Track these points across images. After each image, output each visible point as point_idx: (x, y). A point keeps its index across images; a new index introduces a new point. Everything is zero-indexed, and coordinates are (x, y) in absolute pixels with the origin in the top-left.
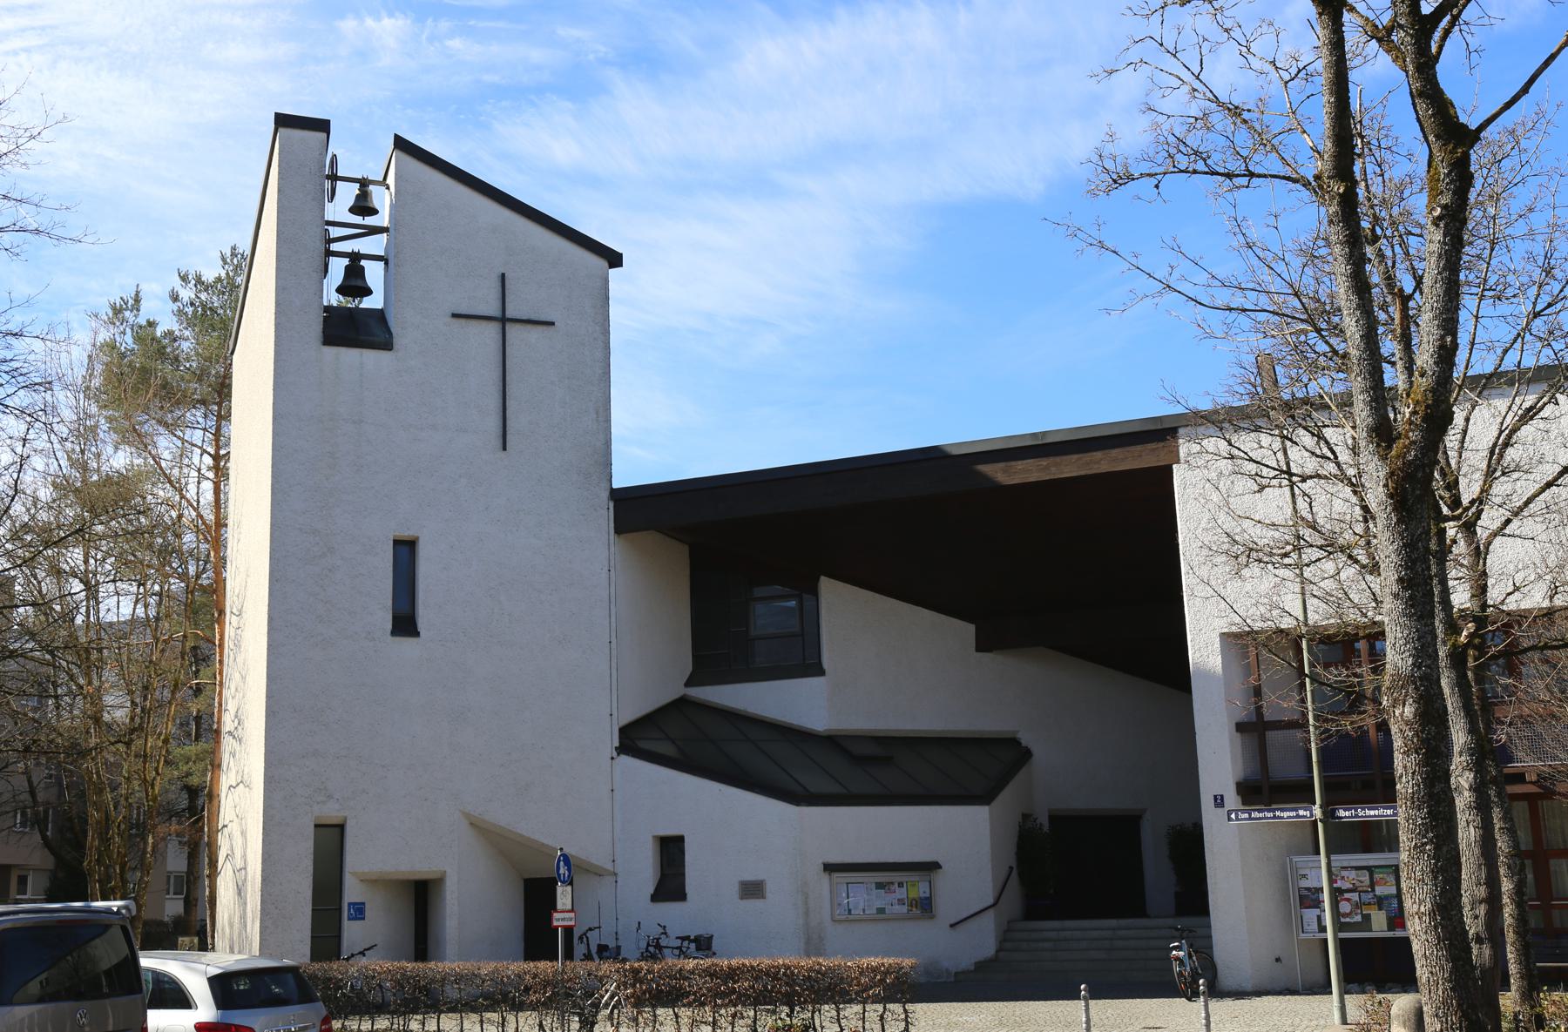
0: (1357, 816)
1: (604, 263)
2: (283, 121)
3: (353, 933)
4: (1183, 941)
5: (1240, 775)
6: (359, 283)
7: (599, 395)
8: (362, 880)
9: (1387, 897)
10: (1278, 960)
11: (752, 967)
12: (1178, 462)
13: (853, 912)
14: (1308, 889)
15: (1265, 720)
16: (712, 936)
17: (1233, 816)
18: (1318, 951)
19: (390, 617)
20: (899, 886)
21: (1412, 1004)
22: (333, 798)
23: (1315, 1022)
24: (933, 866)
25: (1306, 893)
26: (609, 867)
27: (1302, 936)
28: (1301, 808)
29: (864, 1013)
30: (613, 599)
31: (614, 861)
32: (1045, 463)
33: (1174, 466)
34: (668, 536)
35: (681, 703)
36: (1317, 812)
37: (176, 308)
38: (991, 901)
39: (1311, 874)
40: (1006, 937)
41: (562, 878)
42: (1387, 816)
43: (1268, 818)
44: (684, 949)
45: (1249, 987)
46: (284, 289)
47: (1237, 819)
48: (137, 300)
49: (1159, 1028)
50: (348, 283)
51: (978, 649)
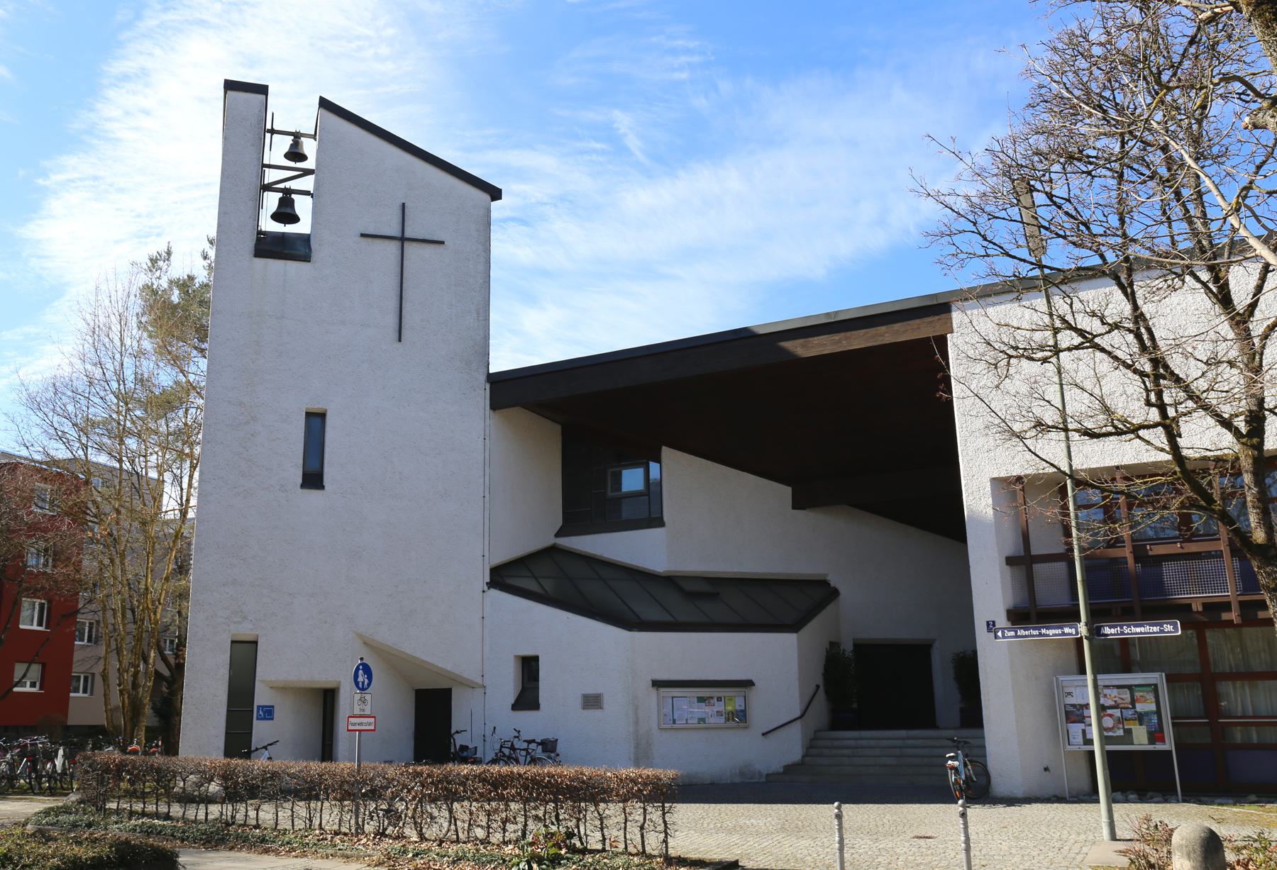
0: (1162, 631)
1: (487, 197)
2: (230, 86)
3: (261, 731)
4: (959, 752)
5: (1010, 603)
6: (289, 211)
7: (480, 299)
8: (271, 687)
9: (1147, 714)
10: (1046, 769)
11: (520, 775)
12: (952, 332)
13: (677, 722)
14: (1074, 706)
15: (1032, 554)
16: (557, 740)
17: (1000, 634)
18: (1083, 764)
19: (300, 473)
20: (718, 700)
21: (1197, 833)
22: (247, 619)
23: (1082, 837)
24: (748, 684)
25: (1072, 709)
26: (479, 680)
27: (1069, 748)
28: (1066, 626)
29: (625, 823)
30: (487, 462)
31: (483, 676)
32: (837, 338)
33: (948, 335)
34: (542, 416)
35: (552, 551)
36: (1082, 629)
37: (206, 264)
38: (798, 714)
39: (1076, 692)
40: (812, 745)
41: (361, 686)
42: (1154, 633)
43: (1034, 636)
44: (530, 751)
45: (1019, 793)
46: (225, 214)
47: (1004, 637)
48: (169, 253)
49: (929, 838)
50: (283, 210)
51: (794, 508)
